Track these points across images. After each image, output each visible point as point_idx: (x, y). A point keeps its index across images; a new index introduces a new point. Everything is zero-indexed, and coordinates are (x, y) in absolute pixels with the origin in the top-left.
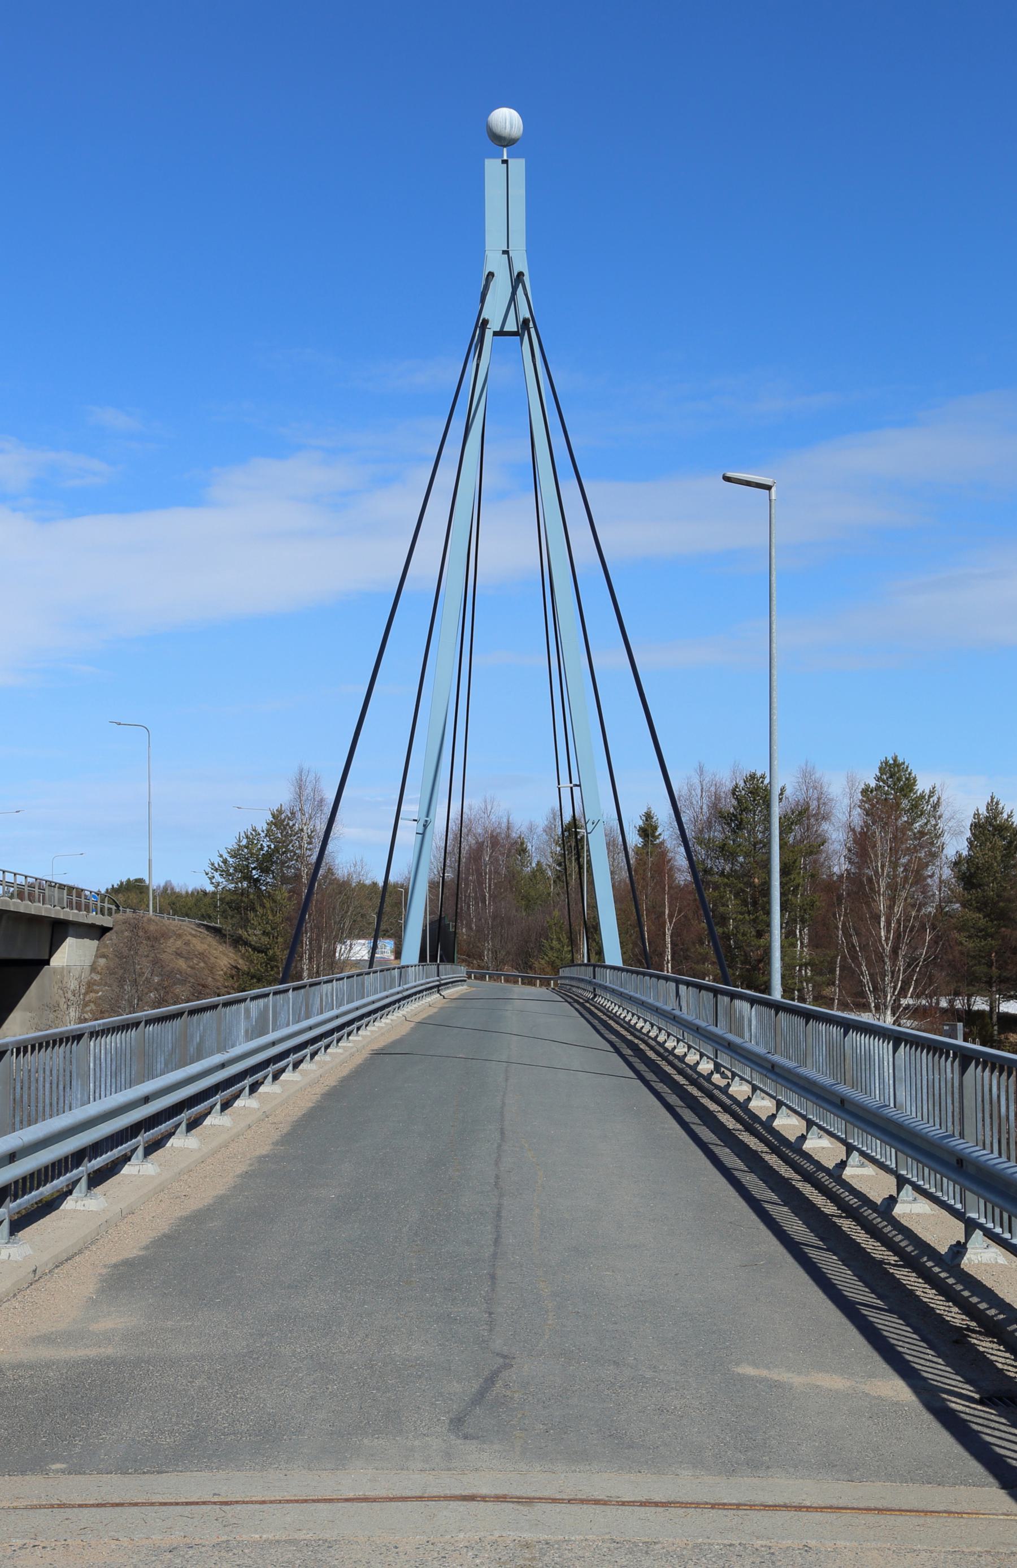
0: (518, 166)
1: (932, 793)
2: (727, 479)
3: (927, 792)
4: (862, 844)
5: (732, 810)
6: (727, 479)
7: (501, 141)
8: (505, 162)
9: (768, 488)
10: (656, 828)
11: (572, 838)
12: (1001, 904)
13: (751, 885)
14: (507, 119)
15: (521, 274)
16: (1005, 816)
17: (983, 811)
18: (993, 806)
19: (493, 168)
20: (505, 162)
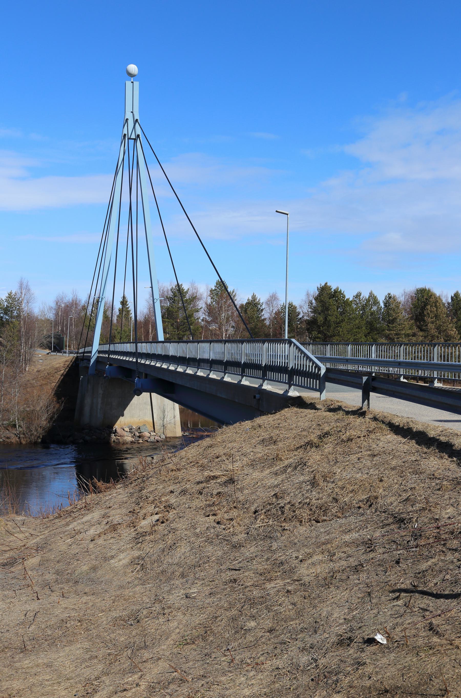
0: (136, 84)
1: (233, 291)
2: (277, 211)
3: (232, 291)
4: (210, 310)
5: (171, 296)
6: (277, 211)
7: (131, 75)
8: (132, 82)
9: (287, 214)
10: (127, 302)
11: (96, 304)
12: (256, 330)
13: (176, 322)
14: (133, 68)
15: (137, 120)
16: (258, 300)
17: (250, 298)
18: (254, 297)
19: (129, 84)
20: (132, 82)
